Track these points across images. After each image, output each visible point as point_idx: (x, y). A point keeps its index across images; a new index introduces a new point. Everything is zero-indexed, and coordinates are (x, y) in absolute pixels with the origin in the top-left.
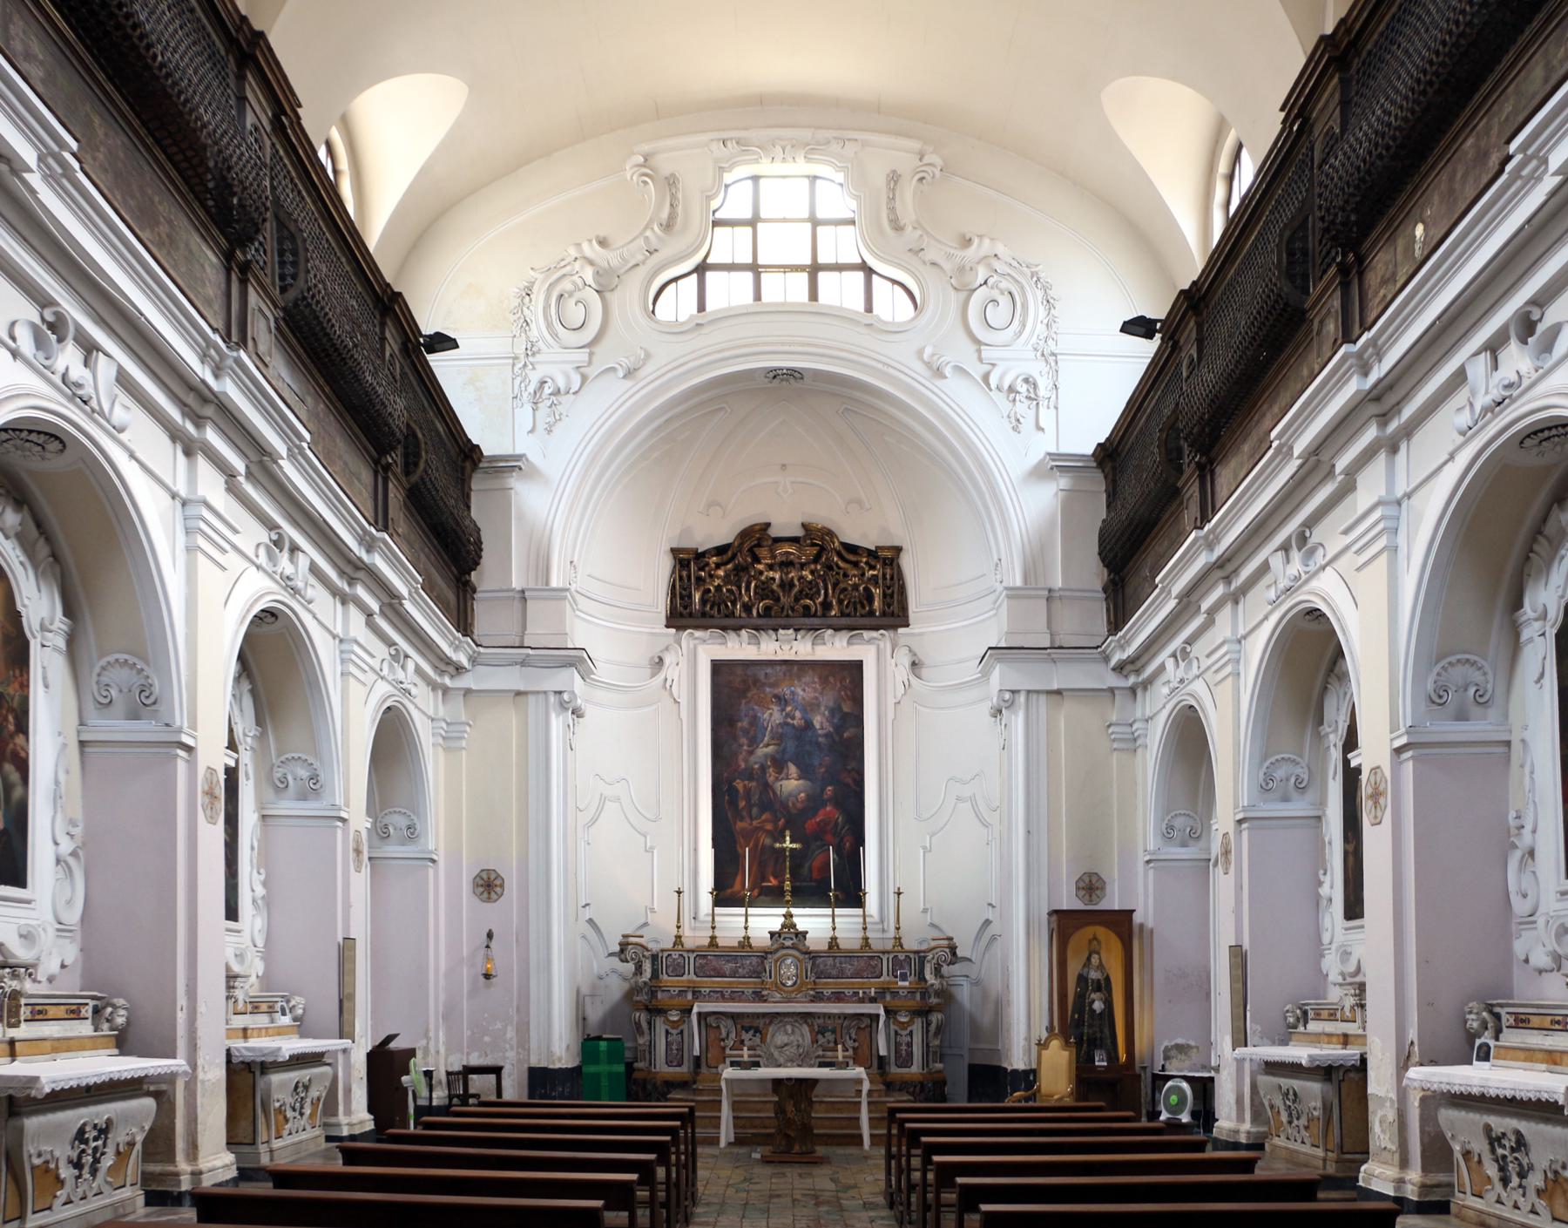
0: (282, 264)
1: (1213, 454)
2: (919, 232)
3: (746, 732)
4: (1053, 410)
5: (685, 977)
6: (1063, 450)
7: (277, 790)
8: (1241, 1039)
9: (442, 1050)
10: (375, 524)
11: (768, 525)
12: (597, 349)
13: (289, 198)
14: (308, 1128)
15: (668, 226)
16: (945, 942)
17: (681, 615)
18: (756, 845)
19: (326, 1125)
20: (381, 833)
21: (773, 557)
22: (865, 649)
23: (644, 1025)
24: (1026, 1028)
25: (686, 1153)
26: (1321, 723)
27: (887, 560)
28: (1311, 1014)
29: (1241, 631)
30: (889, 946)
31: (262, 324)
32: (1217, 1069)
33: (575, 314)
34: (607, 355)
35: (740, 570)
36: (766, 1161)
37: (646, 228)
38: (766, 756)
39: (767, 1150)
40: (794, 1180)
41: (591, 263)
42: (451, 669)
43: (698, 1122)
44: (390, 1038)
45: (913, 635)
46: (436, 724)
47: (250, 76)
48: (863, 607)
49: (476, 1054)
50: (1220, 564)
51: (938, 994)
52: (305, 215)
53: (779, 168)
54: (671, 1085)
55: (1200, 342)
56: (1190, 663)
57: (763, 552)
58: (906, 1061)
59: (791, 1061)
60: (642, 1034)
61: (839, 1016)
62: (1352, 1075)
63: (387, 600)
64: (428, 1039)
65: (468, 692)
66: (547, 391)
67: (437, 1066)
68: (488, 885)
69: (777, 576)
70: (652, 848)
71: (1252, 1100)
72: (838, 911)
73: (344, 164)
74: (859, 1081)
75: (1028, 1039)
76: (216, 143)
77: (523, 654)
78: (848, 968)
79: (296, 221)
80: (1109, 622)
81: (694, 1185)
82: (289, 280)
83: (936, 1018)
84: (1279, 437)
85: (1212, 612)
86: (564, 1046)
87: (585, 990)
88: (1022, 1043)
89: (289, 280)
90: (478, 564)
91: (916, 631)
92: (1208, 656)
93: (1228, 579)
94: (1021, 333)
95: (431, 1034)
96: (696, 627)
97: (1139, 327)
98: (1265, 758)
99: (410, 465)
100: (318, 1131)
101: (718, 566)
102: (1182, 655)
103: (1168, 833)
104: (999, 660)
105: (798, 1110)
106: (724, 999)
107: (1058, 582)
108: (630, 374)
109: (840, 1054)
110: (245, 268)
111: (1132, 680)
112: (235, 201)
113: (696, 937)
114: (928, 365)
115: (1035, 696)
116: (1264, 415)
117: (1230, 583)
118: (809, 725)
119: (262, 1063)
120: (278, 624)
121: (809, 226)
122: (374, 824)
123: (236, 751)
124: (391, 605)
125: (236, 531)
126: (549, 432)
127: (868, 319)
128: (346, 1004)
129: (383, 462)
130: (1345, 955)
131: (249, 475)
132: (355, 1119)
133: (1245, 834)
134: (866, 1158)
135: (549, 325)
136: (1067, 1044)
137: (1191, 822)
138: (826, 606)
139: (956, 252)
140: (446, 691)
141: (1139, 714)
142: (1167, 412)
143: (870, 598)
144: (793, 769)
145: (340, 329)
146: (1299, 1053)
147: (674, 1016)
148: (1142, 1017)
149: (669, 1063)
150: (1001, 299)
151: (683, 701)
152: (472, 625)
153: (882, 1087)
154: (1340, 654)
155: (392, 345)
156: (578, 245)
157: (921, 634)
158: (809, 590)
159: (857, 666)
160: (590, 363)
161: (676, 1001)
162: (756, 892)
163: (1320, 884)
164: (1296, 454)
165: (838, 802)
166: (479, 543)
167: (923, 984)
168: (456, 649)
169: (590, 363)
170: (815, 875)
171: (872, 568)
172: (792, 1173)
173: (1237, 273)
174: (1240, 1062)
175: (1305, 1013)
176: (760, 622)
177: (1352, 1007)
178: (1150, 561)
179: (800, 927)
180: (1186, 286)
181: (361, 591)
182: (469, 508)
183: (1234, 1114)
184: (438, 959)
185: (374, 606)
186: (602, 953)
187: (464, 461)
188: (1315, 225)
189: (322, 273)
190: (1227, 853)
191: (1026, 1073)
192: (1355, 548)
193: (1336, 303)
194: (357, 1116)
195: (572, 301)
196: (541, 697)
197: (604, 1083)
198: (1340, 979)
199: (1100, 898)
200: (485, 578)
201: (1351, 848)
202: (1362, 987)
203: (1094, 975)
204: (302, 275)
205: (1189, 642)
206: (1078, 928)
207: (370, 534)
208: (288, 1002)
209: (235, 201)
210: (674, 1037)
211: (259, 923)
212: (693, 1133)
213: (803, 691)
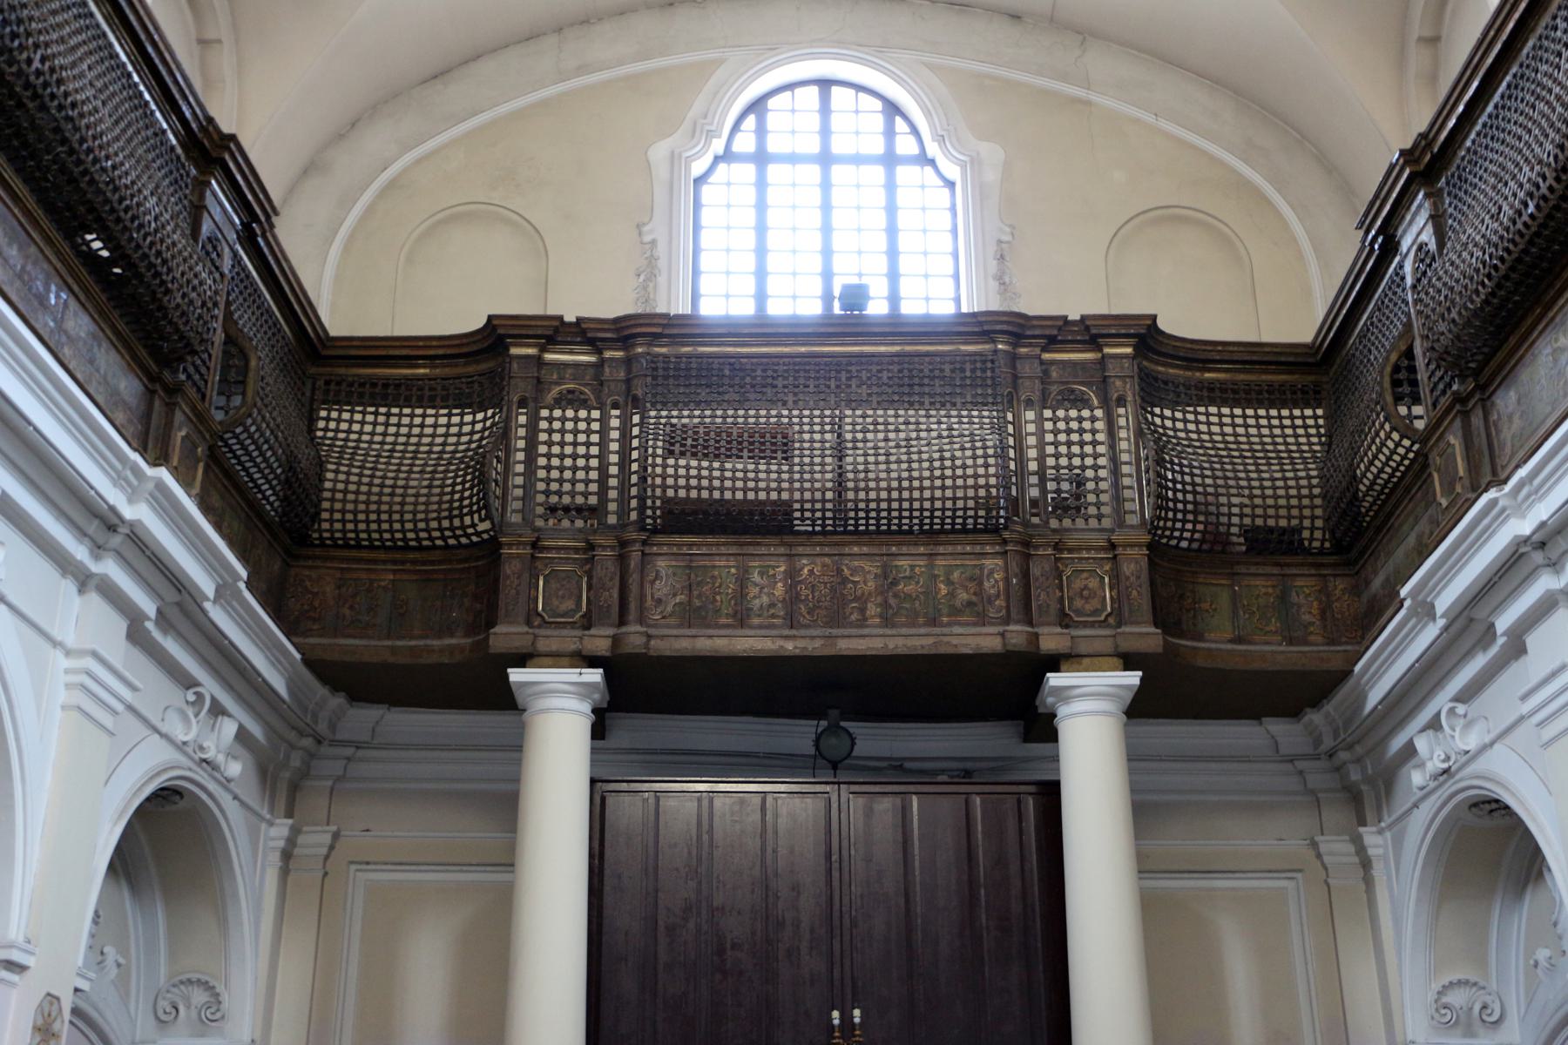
10: (142, 450)
63: (171, 595)
185: (148, 606)
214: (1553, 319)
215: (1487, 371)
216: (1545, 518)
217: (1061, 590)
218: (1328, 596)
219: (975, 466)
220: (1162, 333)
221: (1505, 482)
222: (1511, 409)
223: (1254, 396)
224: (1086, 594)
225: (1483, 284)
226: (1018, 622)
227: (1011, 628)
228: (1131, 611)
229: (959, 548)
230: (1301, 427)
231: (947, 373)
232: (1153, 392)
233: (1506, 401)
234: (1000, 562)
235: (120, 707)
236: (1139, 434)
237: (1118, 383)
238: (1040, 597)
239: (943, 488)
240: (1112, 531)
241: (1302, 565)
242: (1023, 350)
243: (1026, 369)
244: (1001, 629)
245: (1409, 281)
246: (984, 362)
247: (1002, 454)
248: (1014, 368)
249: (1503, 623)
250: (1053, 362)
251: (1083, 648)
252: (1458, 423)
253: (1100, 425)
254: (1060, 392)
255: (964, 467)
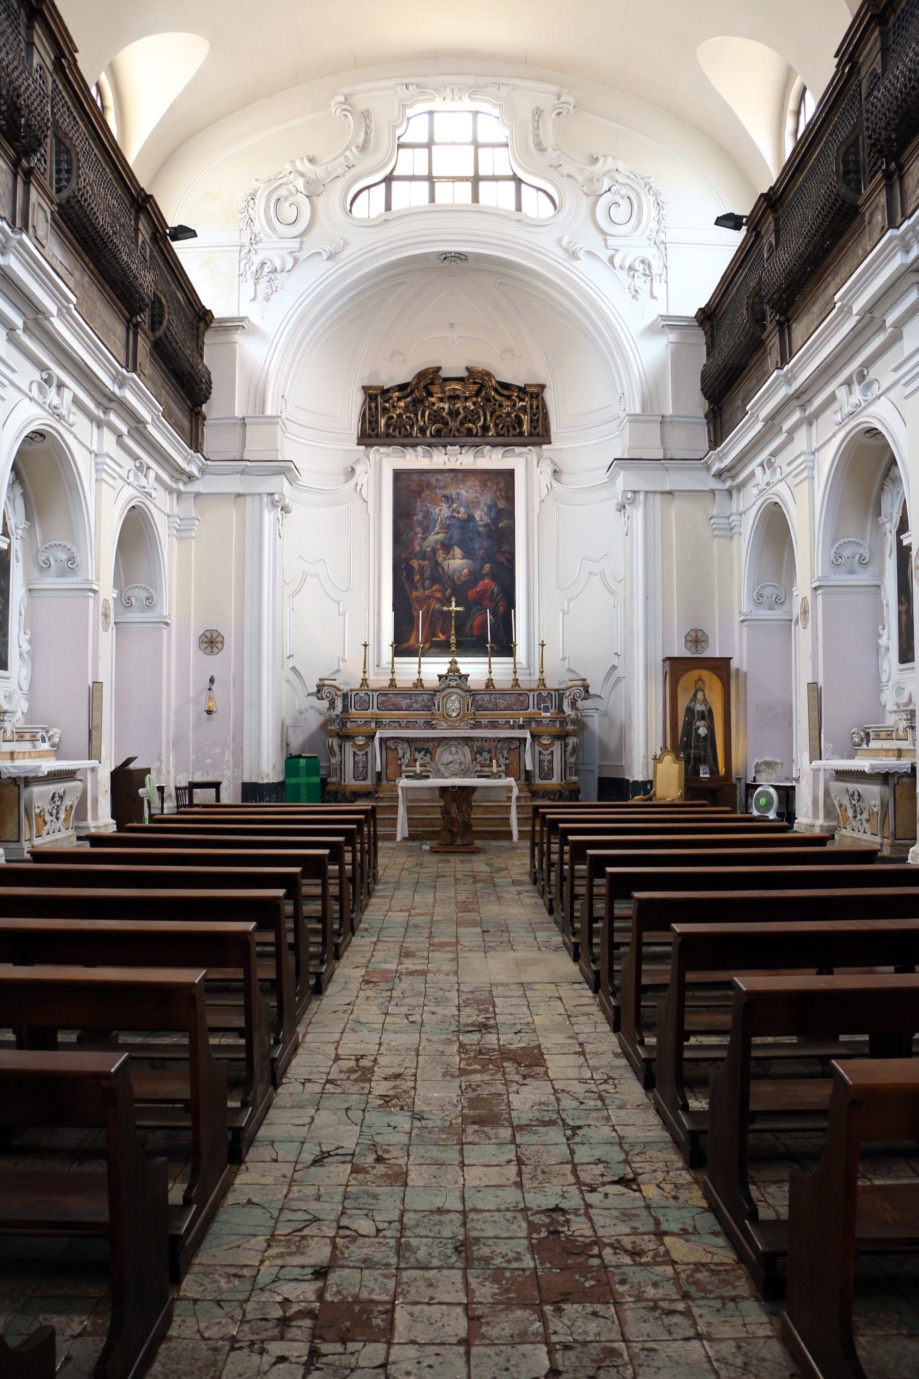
0: (59, 171)
1: (789, 314)
2: (557, 153)
3: (420, 523)
4: (663, 283)
5: (370, 711)
6: (671, 313)
7: (41, 569)
8: (817, 754)
9: (172, 771)
10: (126, 367)
11: (439, 368)
12: (305, 239)
13: (66, 123)
14: (63, 829)
15: (363, 148)
16: (580, 683)
17: (369, 436)
18: (428, 610)
19: (77, 828)
20: (124, 602)
21: (443, 392)
22: (516, 460)
23: (336, 749)
24: (645, 752)
25: (369, 843)
26: (879, 514)
27: (534, 395)
28: (872, 735)
29: (815, 446)
30: (535, 686)
31: (41, 215)
32: (797, 780)
33: (289, 213)
34: (312, 243)
35: (417, 402)
36: (434, 851)
37: (346, 149)
38: (437, 541)
39: (434, 843)
40: (457, 865)
41: (302, 175)
42: (185, 478)
43: (379, 822)
44: (130, 760)
45: (554, 450)
46: (171, 519)
47: (37, 27)
48: (515, 429)
49: (200, 773)
50: (798, 395)
51: (573, 722)
52: (78, 135)
53: (448, 105)
54: (356, 795)
55: (777, 232)
56: (775, 470)
57: (435, 389)
58: (547, 774)
59: (455, 775)
60: (334, 755)
61: (494, 739)
62: (905, 780)
63: (133, 424)
64: (161, 761)
65: (197, 495)
66: (266, 270)
67: (168, 785)
68: (211, 642)
69: (446, 406)
70: (344, 612)
71: (825, 801)
72: (493, 659)
73: (110, 101)
74: (509, 789)
75: (646, 757)
76: (8, 75)
77: (242, 465)
78: (502, 703)
79: (71, 139)
80: (710, 441)
81: (375, 868)
82: (64, 183)
83: (572, 741)
84: (841, 299)
85: (791, 432)
86: (271, 766)
87: (288, 722)
88: (642, 760)
89: (64, 183)
90: (207, 398)
91: (557, 447)
92: (789, 464)
93: (803, 407)
94: (637, 227)
95: (163, 758)
96: (382, 445)
97: (729, 221)
98: (835, 541)
99: (156, 322)
100: (71, 832)
101: (399, 399)
102: (768, 465)
103: (759, 599)
104: (623, 468)
105: (460, 811)
106: (401, 727)
107: (669, 411)
108: (331, 257)
109: (495, 769)
110: (28, 173)
111: (728, 484)
112: (23, 121)
113: (379, 680)
114: (566, 250)
115: (651, 495)
116: (829, 284)
117: (805, 410)
118: (471, 518)
119: (26, 778)
120: (45, 443)
121: (472, 148)
122: (120, 595)
123: (9, 538)
124: (137, 428)
125: (14, 371)
126: (267, 300)
127: (518, 216)
128: (94, 733)
129: (134, 321)
130: (900, 690)
131: (26, 329)
132: (101, 823)
133: (820, 598)
134: (515, 848)
135: (269, 222)
136: (677, 758)
137: (777, 592)
138: (485, 428)
139: (586, 168)
140: (180, 494)
141: (734, 510)
142: (752, 284)
143: (520, 422)
144: (458, 551)
145: (103, 220)
146: (863, 764)
147: (360, 741)
148: (737, 730)
149: (356, 778)
150: (621, 202)
151: (371, 500)
152: (202, 444)
153: (529, 794)
154: (893, 462)
155: (144, 233)
156: (293, 162)
157: (560, 450)
158: (472, 417)
159: (510, 474)
160: (301, 249)
161: (362, 729)
162: (428, 645)
163: (880, 636)
164: (855, 312)
165: (494, 577)
166: (209, 383)
167: (562, 715)
168: (189, 462)
169: (301, 249)
170: (475, 632)
171: (522, 400)
172: (455, 860)
173: (805, 181)
174: (816, 771)
175: (868, 734)
176: (433, 440)
177: (905, 729)
178: (741, 394)
179: (463, 672)
180: (765, 190)
181: (113, 417)
182: (202, 357)
183: (811, 813)
184: (170, 699)
185: (124, 429)
186: (302, 693)
187: (198, 322)
188: (864, 142)
189: (90, 178)
190: (805, 612)
191: (645, 783)
192: (903, 382)
193: (883, 199)
194: (102, 820)
195: (288, 203)
196: (257, 497)
197: (303, 791)
198: (895, 708)
199: (704, 649)
200: (212, 409)
201: (904, 608)
202: (913, 713)
203: (699, 707)
204: (74, 180)
205: (773, 454)
206: (686, 671)
207: (122, 375)
208: (47, 732)
209: (23, 121)
210: (360, 757)
211: (25, 672)
212: (375, 831)
213: (466, 492)
235: (116, 476)
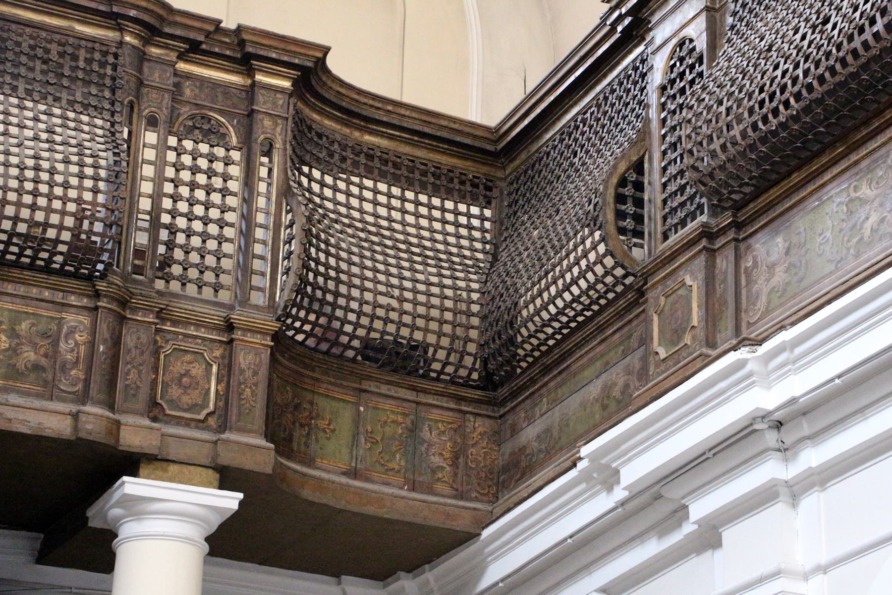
214: (856, 163)
215: (752, 207)
216: (797, 394)
217: (156, 372)
218: (464, 437)
219: (80, 188)
220: (328, 72)
221: (760, 343)
222: (774, 258)
223: (417, 175)
224: (184, 381)
225: (787, 104)
226: (98, 403)
227: (88, 408)
228: (240, 414)
229: (34, 292)
230: (465, 223)
231: (54, 56)
232: (306, 147)
233: (769, 247)
234: (85, 320)
236: (286, 192)
237: (267, 122)
238: (131, 375)
239: (33, 207)
240: (231, 308)
241: (442, 394)
242: (155, 51)
243: (155, 76)
244: (74, 408)
245: (657, 78)
246: (105, 54)
247: (114, 179)
248: (140, 70)
249: (701, 508)
250: (188, 76)
251: (175, 451)
252: (701, 260)
253: (235, 170)
254: (192, 117)
255: (66, 186)
